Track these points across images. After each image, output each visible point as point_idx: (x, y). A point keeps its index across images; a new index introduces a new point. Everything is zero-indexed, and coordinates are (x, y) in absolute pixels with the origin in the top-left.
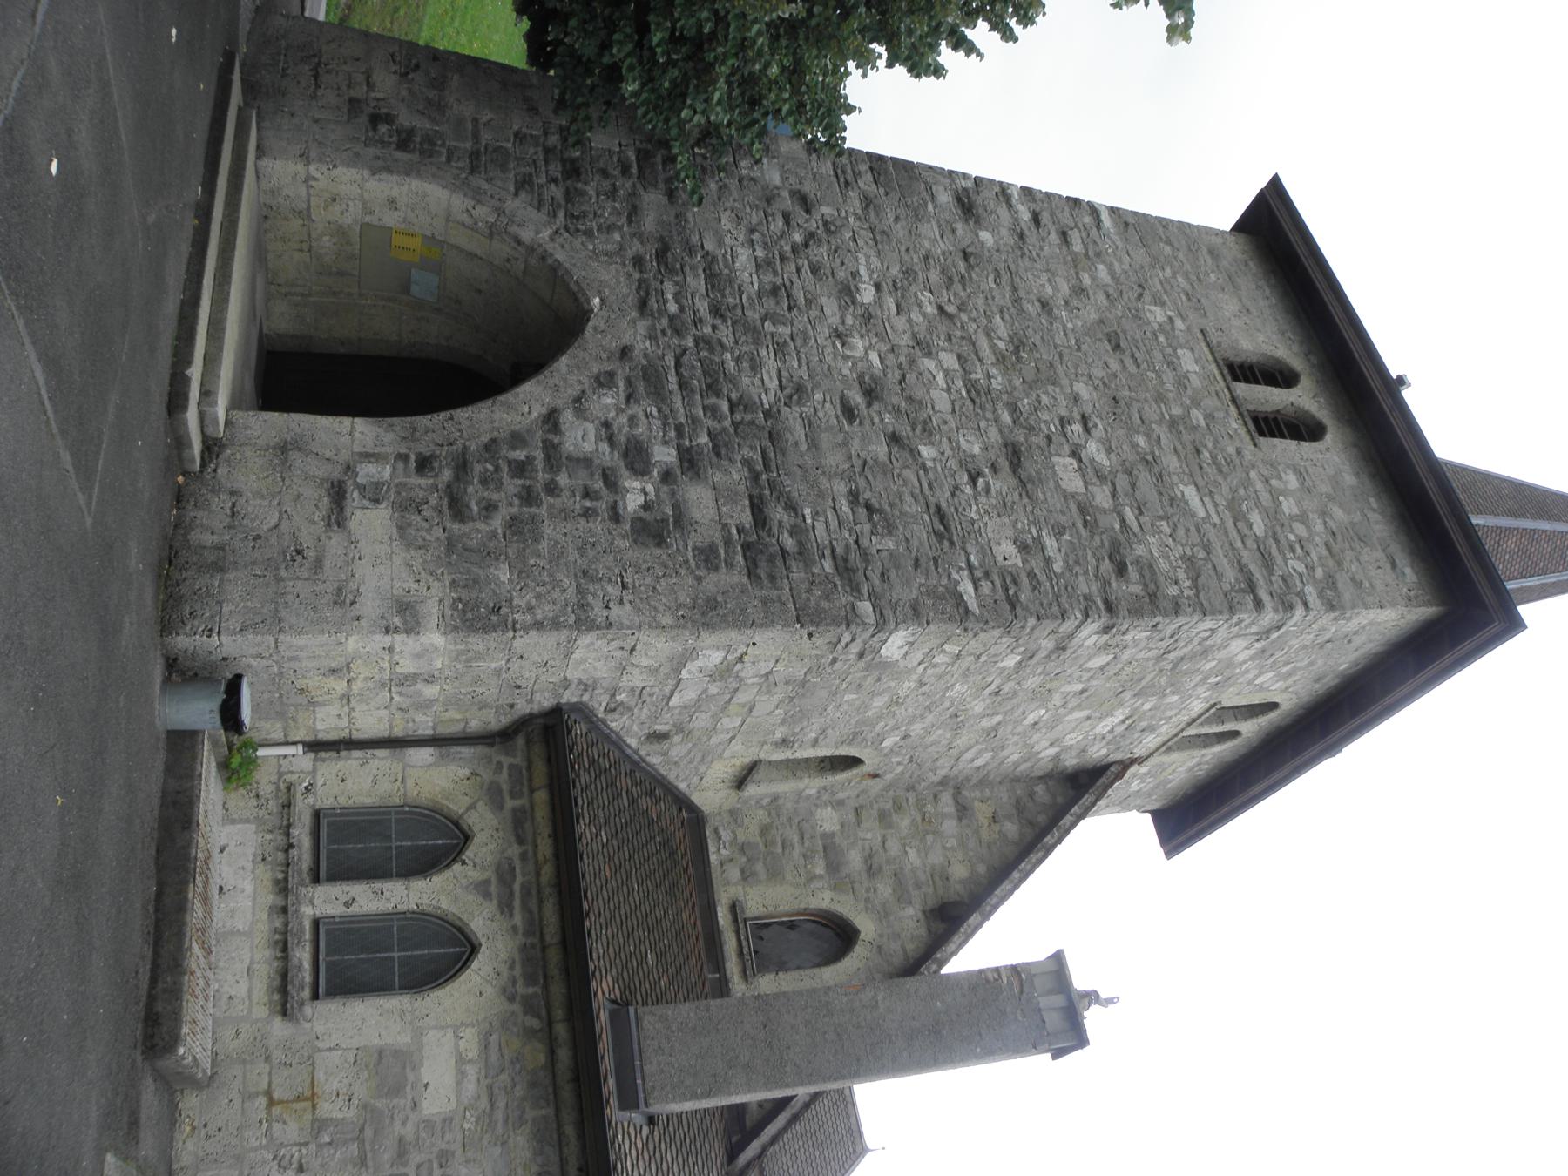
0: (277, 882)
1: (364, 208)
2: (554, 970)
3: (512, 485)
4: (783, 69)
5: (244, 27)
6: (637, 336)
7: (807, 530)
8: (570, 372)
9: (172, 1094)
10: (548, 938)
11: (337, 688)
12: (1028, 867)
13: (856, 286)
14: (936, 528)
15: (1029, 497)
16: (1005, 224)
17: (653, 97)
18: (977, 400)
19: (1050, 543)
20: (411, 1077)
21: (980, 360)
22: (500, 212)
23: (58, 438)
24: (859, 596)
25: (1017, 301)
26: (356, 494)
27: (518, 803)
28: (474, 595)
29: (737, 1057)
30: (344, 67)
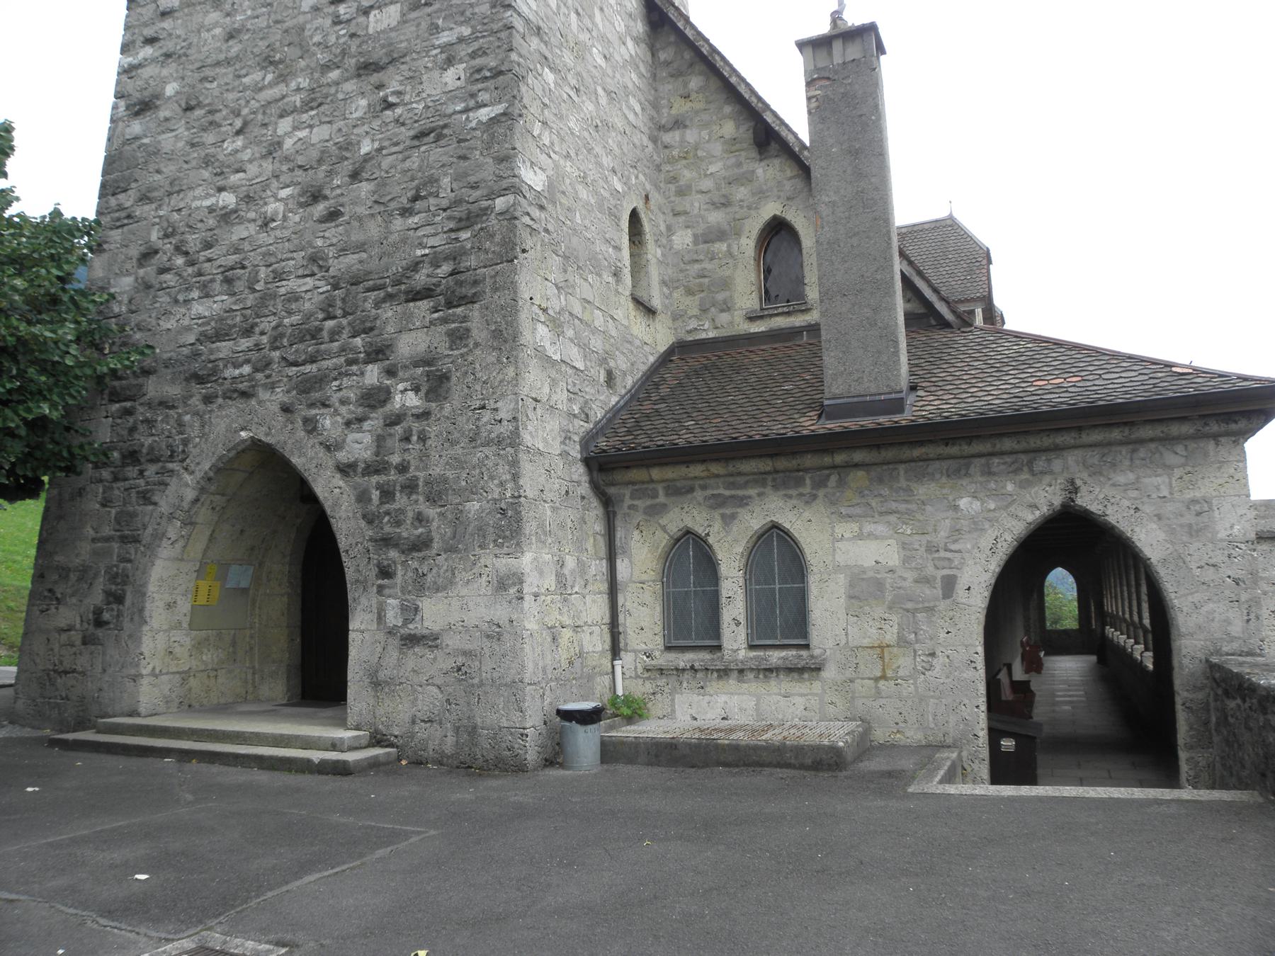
0: (720, 677)
1: (176, 628)
2: (794, 463)
3: (401, 500)
4: (19, 274)
5: (27, 732)
6: (271, 400)
7: (435, 253)
8: (305, 455)
9: (873, 748)
10: (768, 469)
11: (568, 636)
12: (727, 68)
13: (221, 209)
14: (432, 140)
15: (405, 56)
16: (157, 70)
17: (56, 390)
18: (319, 100)
19: (445, 38)
20: (871, 574)
21: (284, 97)
22: (171, 517)
23: (365, 859)
24: (492, 208)
25: (228, 62)
26: (411, 626)
27: (661, 492)
28: (491, 530)
29: (868, 318)
30: (56, 650)
